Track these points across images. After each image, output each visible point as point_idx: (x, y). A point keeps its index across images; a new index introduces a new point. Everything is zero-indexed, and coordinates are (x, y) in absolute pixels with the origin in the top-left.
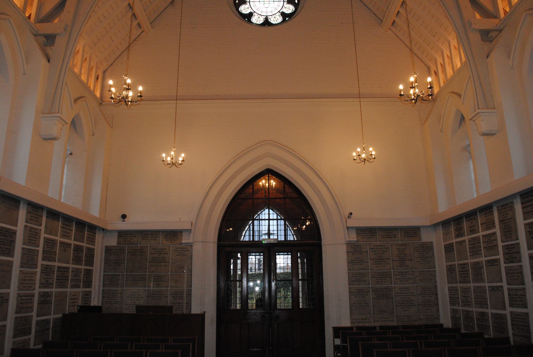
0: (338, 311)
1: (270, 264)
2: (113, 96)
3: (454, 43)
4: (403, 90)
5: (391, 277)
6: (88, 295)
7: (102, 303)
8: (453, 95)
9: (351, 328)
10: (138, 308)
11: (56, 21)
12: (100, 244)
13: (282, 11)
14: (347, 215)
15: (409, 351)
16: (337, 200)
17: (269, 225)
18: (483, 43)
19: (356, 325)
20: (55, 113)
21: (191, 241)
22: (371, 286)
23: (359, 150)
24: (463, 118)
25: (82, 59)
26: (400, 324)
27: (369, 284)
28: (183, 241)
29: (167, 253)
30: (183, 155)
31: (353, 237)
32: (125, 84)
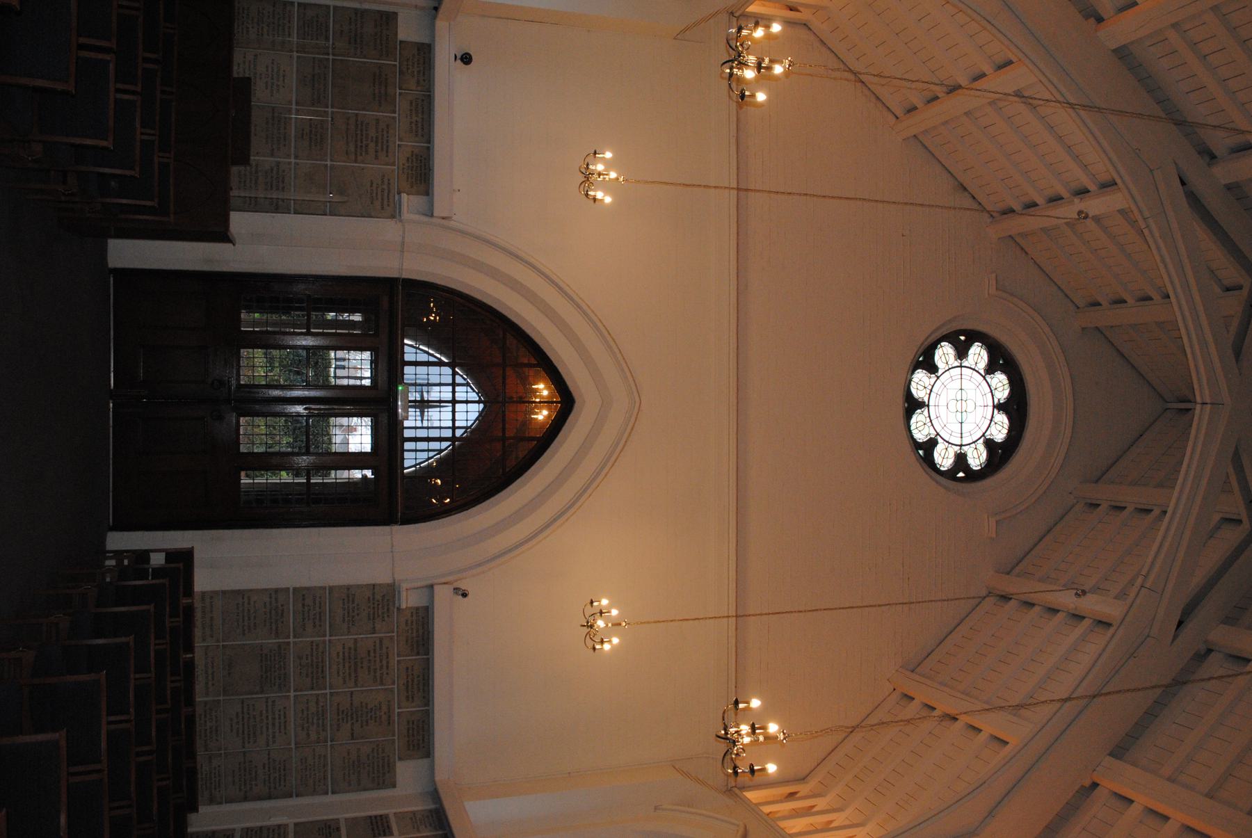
0: (230, 562)
1: (353, 401)
2: (745, 32)
4: (748, 709)
5: (312, 689)
8: (742, 829)
10: (245, 85)
13: (940, 440)
17: (444, 407)
19: (198, 605)
21: (406, 215)
22: (291, 640)
26: (199, 710)
27: (295, 637)
28: (404, 196)
29: (376, 157)
30: (608, 200)
31: (409, 600)
32: (771, 61)
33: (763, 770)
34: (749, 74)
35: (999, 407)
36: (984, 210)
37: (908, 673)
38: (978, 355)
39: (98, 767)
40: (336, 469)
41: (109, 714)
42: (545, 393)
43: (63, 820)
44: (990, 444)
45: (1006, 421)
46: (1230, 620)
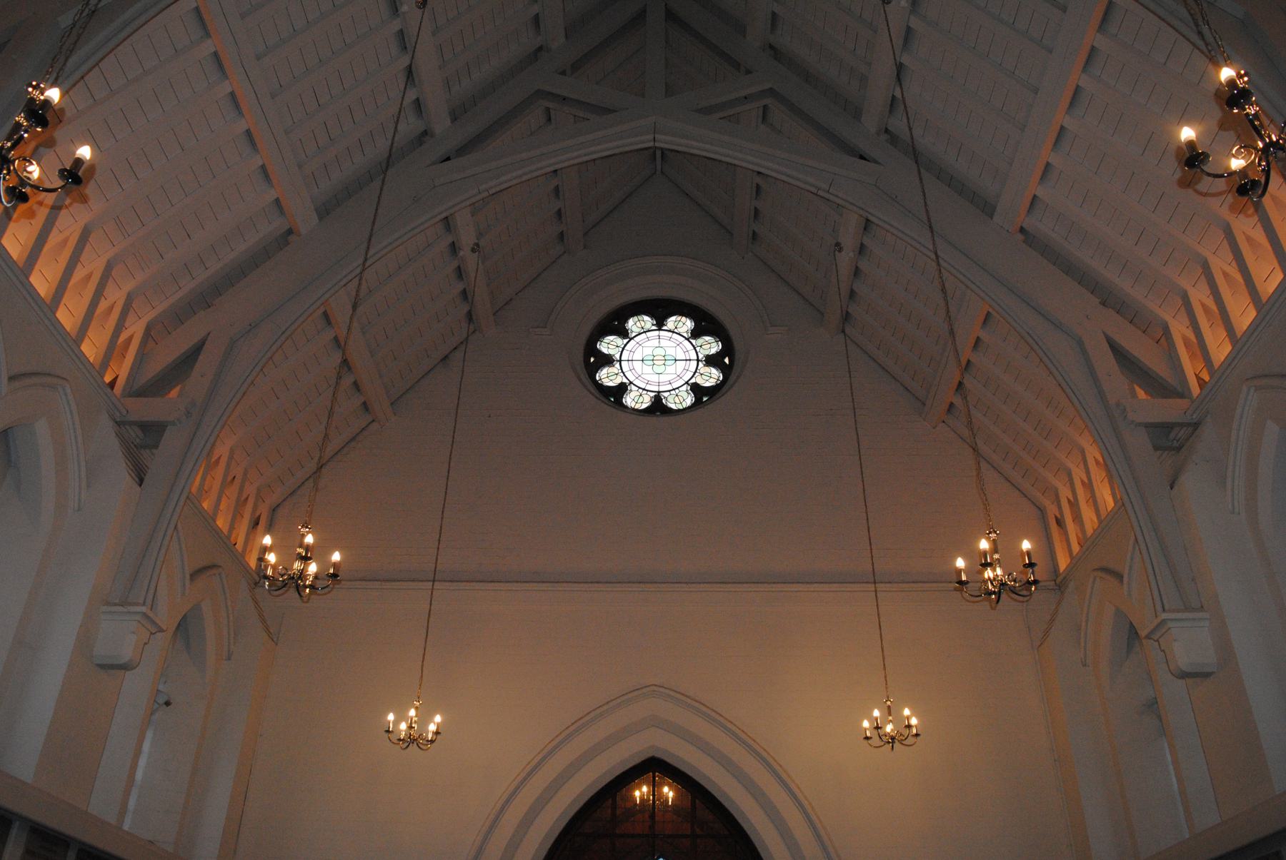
2: (270, 572)
3: (1093, 453)
4: (967, 571)
8: (1099, 574)
11: (174, 393)
13: (693, 381)
18: (1159, 453)
20: (137, 604)
23: (876, 713)
24: (1133, 633)
25: (226, 476)
30: (438, 718)
32: (301, 546)
34: (313, 568)
35: (660, 325)
42: (645, 789)
44: (696, 334)
45: (673, 318)
46: (857, 114)
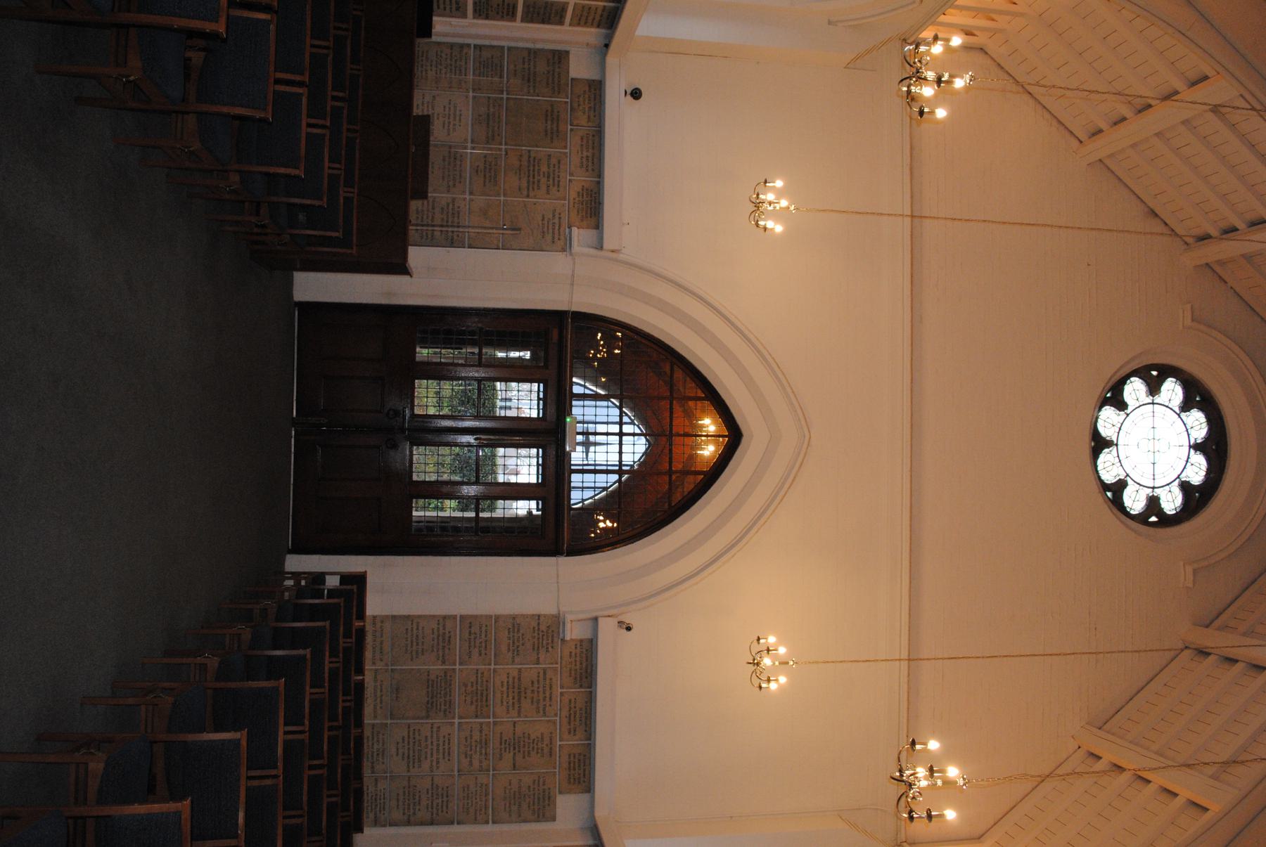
0: (400, 588)
1: (517, 433)
2: (922, 48)
4: (925, 751)
6: (457, 9)
7: (439, 43)
9: (361, 615)
10: (425, 121)
12: (574, 39)
14: (627, 619)
15: (301, 816)
16: (667, 594)
17: (609, 443)
19: (369, 627)
21: (576, 248)
22: (457, 667)
26: (367, 732)
27: (461, 664)
28: (575, 230)
29: (548, 193)
30: (779, 229)
31: (574, 632)
32: (951, 76)
33: (942, 816)
34: (928, 91)
35: (1197, 447)
36: (1177, 235)
37: (1095, 730)
38: (1172, 391)
39: (273, 772)
40: (505, 498)
41: (285, 724)
43: (241, 815)
44: (1185, 487)
